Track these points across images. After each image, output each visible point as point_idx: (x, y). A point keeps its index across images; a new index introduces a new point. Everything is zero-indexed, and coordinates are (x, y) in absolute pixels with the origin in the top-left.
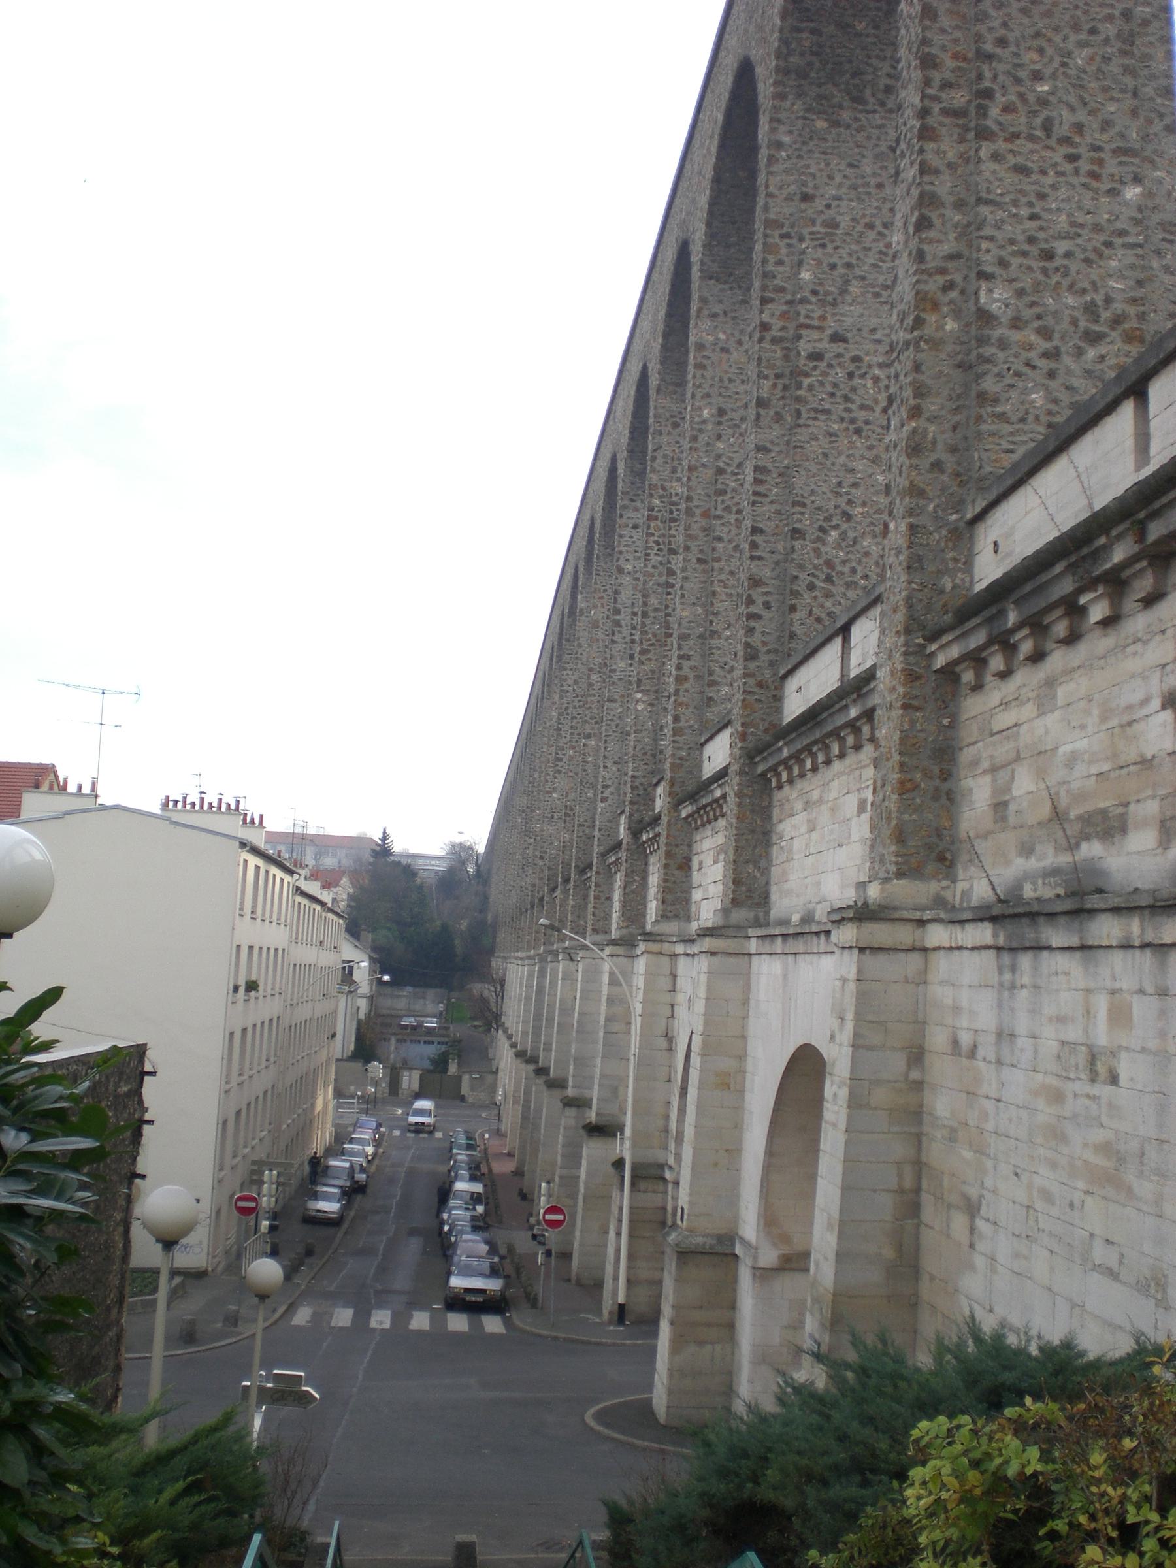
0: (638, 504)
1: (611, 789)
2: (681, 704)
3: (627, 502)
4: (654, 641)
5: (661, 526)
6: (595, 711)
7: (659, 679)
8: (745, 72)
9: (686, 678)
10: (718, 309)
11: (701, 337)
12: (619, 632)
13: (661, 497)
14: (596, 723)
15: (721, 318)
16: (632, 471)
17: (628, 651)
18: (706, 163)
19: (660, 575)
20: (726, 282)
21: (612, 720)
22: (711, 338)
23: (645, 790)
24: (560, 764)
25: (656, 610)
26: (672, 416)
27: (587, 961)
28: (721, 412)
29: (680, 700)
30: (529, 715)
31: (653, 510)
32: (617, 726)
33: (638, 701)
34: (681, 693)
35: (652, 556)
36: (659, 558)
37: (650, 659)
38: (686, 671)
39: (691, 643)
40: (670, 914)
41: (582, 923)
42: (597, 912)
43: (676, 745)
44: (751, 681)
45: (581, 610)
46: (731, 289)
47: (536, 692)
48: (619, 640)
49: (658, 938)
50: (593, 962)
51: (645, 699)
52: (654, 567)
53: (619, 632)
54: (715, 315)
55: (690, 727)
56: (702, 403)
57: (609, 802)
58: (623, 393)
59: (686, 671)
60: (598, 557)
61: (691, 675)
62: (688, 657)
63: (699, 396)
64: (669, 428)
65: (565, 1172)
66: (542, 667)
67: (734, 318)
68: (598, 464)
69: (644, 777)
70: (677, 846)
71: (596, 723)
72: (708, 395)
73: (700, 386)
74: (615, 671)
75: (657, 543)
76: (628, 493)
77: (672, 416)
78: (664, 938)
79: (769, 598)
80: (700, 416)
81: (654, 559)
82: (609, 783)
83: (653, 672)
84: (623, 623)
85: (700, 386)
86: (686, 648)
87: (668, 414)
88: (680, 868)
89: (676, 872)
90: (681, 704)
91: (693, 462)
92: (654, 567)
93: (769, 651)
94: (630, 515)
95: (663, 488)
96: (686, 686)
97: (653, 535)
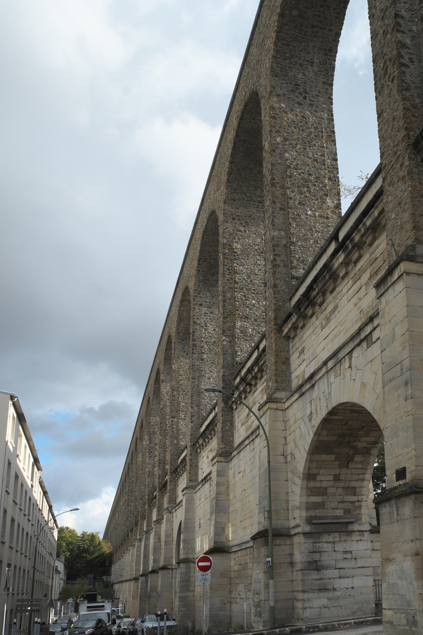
0: (201, 295)
1: (196, 417)
2: (277, 279)
3: (197, 294)
4: (229, 313)
5: (230, 262)
6: (176, 406)
7: (233, 330)
8: (187, 290)
9: (278, 266)
10: (280, 92)
11: (273, 104)
12: (196, 349)
13: (229, 249)
14: (177, 411)
15: (282, 97)
16: (199, 280)
17: (200, 357)
18: (196, 254)
19: (231, 284)
20: (284, 80)
21: (194, 387)
22: (278, 106)
23: (230, 382)
24: (151, 454)
25: (230, 299)
26: (232, 215)
27: (188, 495)
28: (286, 139)
29: (276, 276)
30: (125, 472)
31: (225, 255)
32: (197, 389)
33: (223, 341)
34: (277, 273)
35: (226, 275)
36: (230, 276)
37: (228, 322)
38: (278, 262)
39: (280, 249)
40: (280, 388)
41: (174, 496)
42: (191, 472)
43: (276, 299)
44: (408, 103)
45: (163, 380)
46: (286, 83)
47: (123, 478)
48: (196, 353)
49: (275, 400)
50: (191, 495)
51: (227, 339)
52: (227, 280)
53: (196, 349)
54: (279, 95)
55: (284, 290)
56: (276, 135)
57: (195, 422)
58: (138, 427)
59: (278, 262)
60: (175, 343)
61: (281, 265)
62: (279, 256)
63: (274, 131)
64: (231, 220)
65: (182, 595)
66: (128, 462)
67: (288, 98)
68: (151, 376)
69: (229, 376)
70: (281, 352)
71: (177, 411)
72: (279, 131)
73: (274, 127)
74: (195, 365)
75: (229, 270)
76: (197, 290)
77: (232, 215)
78: (279, 400)
79: (412, 56)
80: (275, 141)
81: (228, 277)
82: (194, 414)
83: (230, 327)
84: (197, 345)
85: (274, 127)
86: (277, 251)
87: (230, 213)
88: (284, 363)
89: (282, 366)
90: (277, 279)
91: (273, 162)
92: (227, 280)
93: (416, 87)
94: (198, 300)
95: (230, 245)
96: (279, 270)
97: (226, 266)
